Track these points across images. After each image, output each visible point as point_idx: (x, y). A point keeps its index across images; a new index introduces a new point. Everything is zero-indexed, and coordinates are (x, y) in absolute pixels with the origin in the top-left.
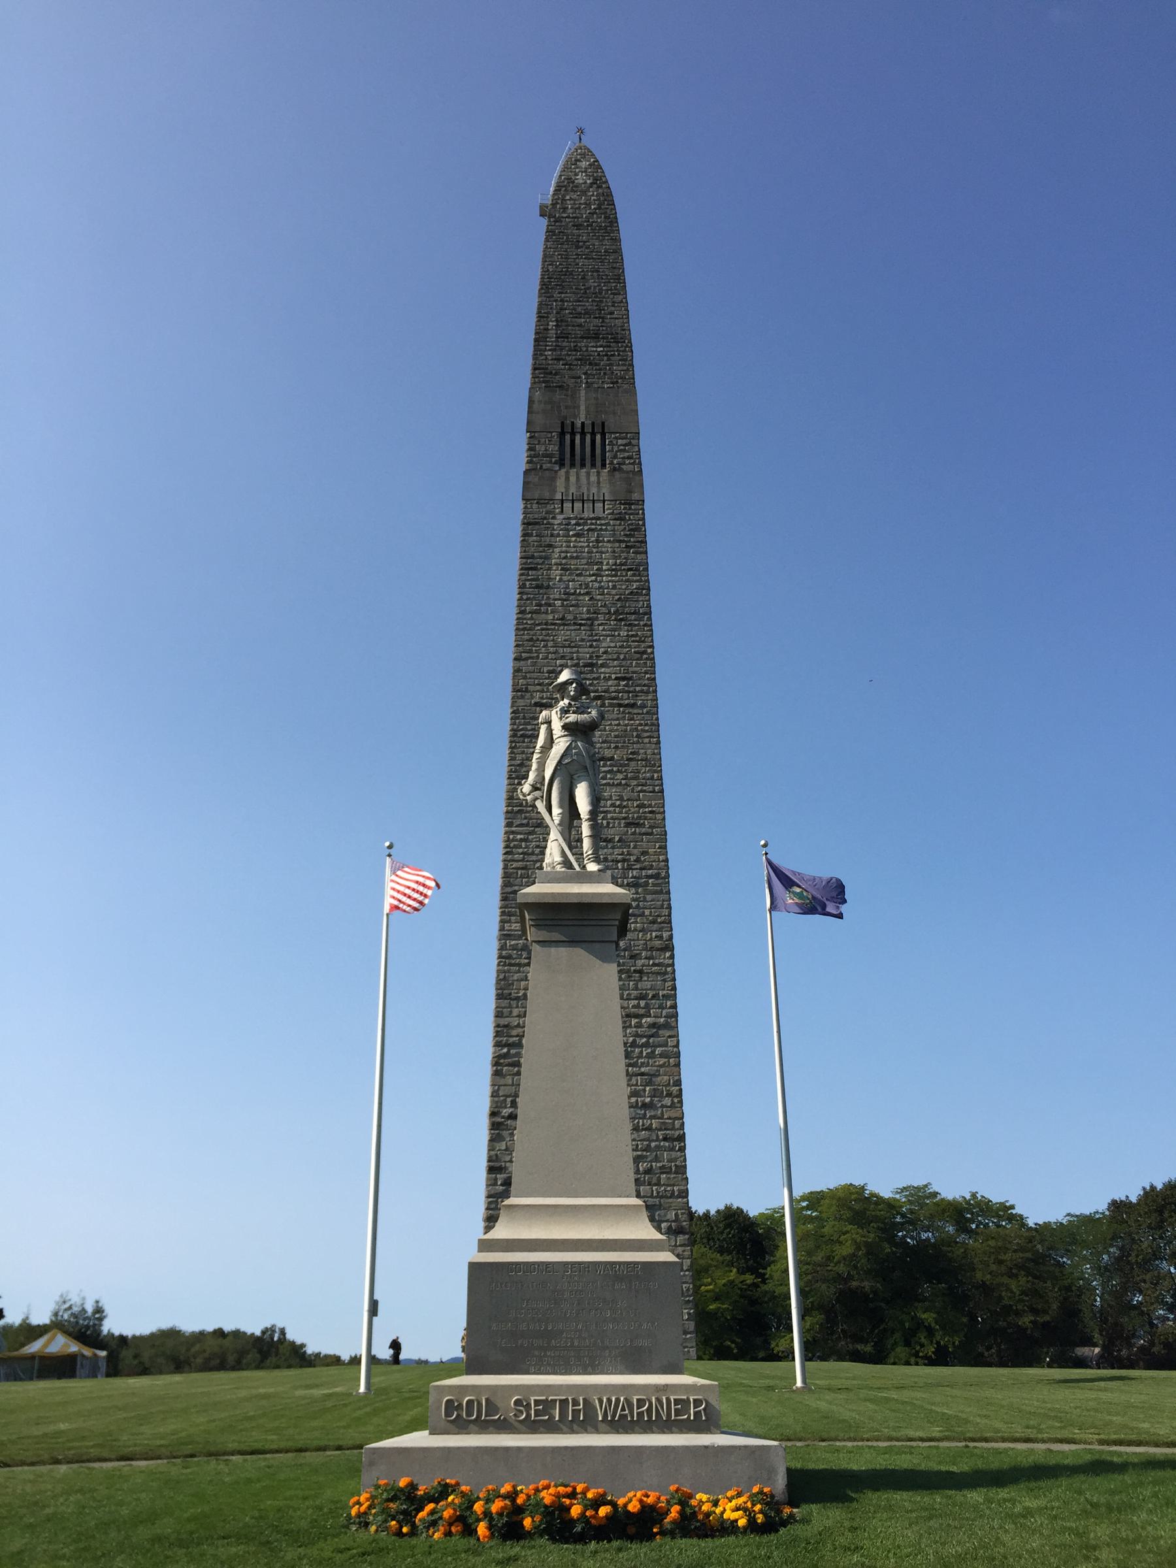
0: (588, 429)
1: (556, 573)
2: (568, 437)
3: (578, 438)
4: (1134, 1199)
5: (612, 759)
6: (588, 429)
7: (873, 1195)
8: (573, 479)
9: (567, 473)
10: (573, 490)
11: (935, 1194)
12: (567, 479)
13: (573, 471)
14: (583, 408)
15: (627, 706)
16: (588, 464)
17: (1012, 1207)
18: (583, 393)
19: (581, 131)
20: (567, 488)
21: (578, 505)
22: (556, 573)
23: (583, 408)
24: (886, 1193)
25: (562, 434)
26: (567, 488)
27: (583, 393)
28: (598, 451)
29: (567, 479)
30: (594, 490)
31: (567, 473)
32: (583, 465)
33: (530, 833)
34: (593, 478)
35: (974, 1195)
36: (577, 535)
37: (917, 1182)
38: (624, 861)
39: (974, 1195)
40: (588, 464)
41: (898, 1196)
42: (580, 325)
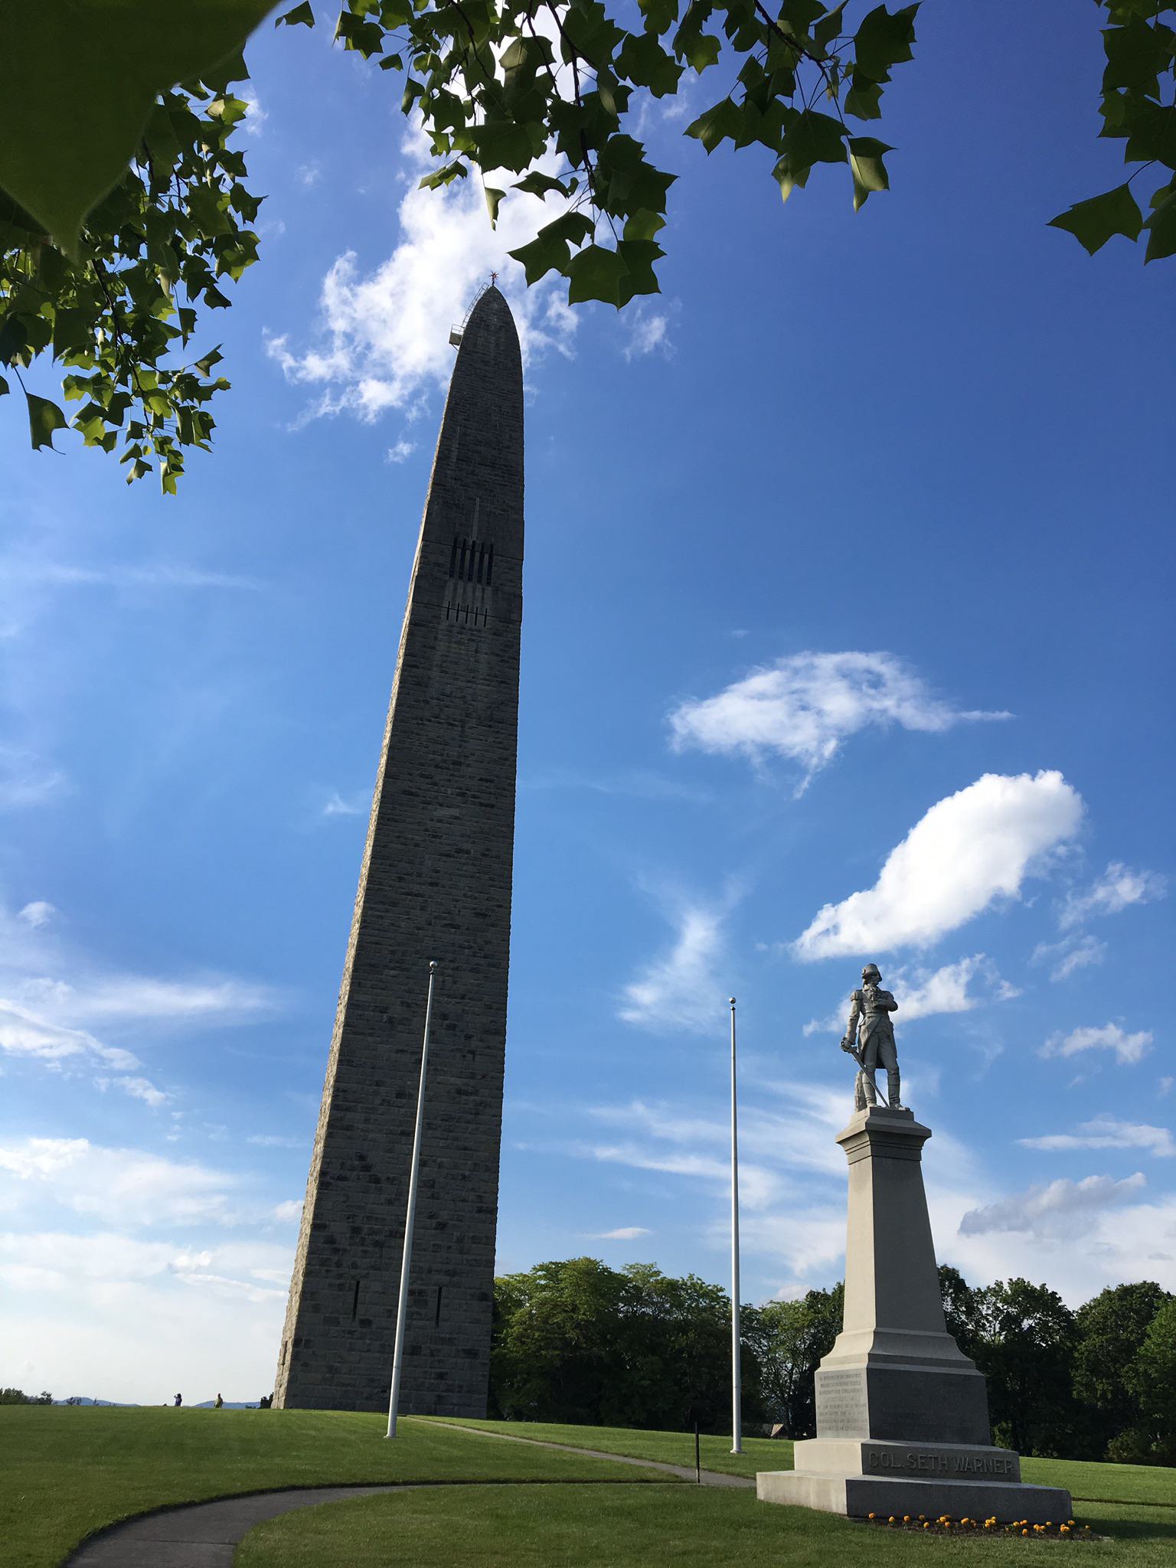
0: (478, 548)
1: (435, 673)
2: (459, 551)
3: (468, 552)
4: (829, 1292)
5: (468, 852)
6: (478, 548)
7: (605, 1270)
8: (460, 591)
9: (455, 585)
10: (459, 600)
11: (658, 1273)
12: (455, 589)
13: (470, 584)
14: (475, 528)
15: (487, 806)
16: (475, 578)
17: (722, 1290)
18: (477, 515)
19: (494, 276)
20: (454, 598)
21: (462, 615)
22: (435, 673)
23: (475, 528)
24: (616, 1269)
25: (455, 547)
26: (454, 598)
27: (477, 515)
28: (476, 567)
29: (455, 589)
30: (478, 604)
31: (455, 585)
32: (470, 579)
33: (387, 911)
34: (478, 594)
35: (691, 1277)
36: (459, 643)
37: (646, 1262)
38: (470, 947)
39: (691, 1277)
40: (475, 578)
41: (625, 1273)
42: (479, 452)
